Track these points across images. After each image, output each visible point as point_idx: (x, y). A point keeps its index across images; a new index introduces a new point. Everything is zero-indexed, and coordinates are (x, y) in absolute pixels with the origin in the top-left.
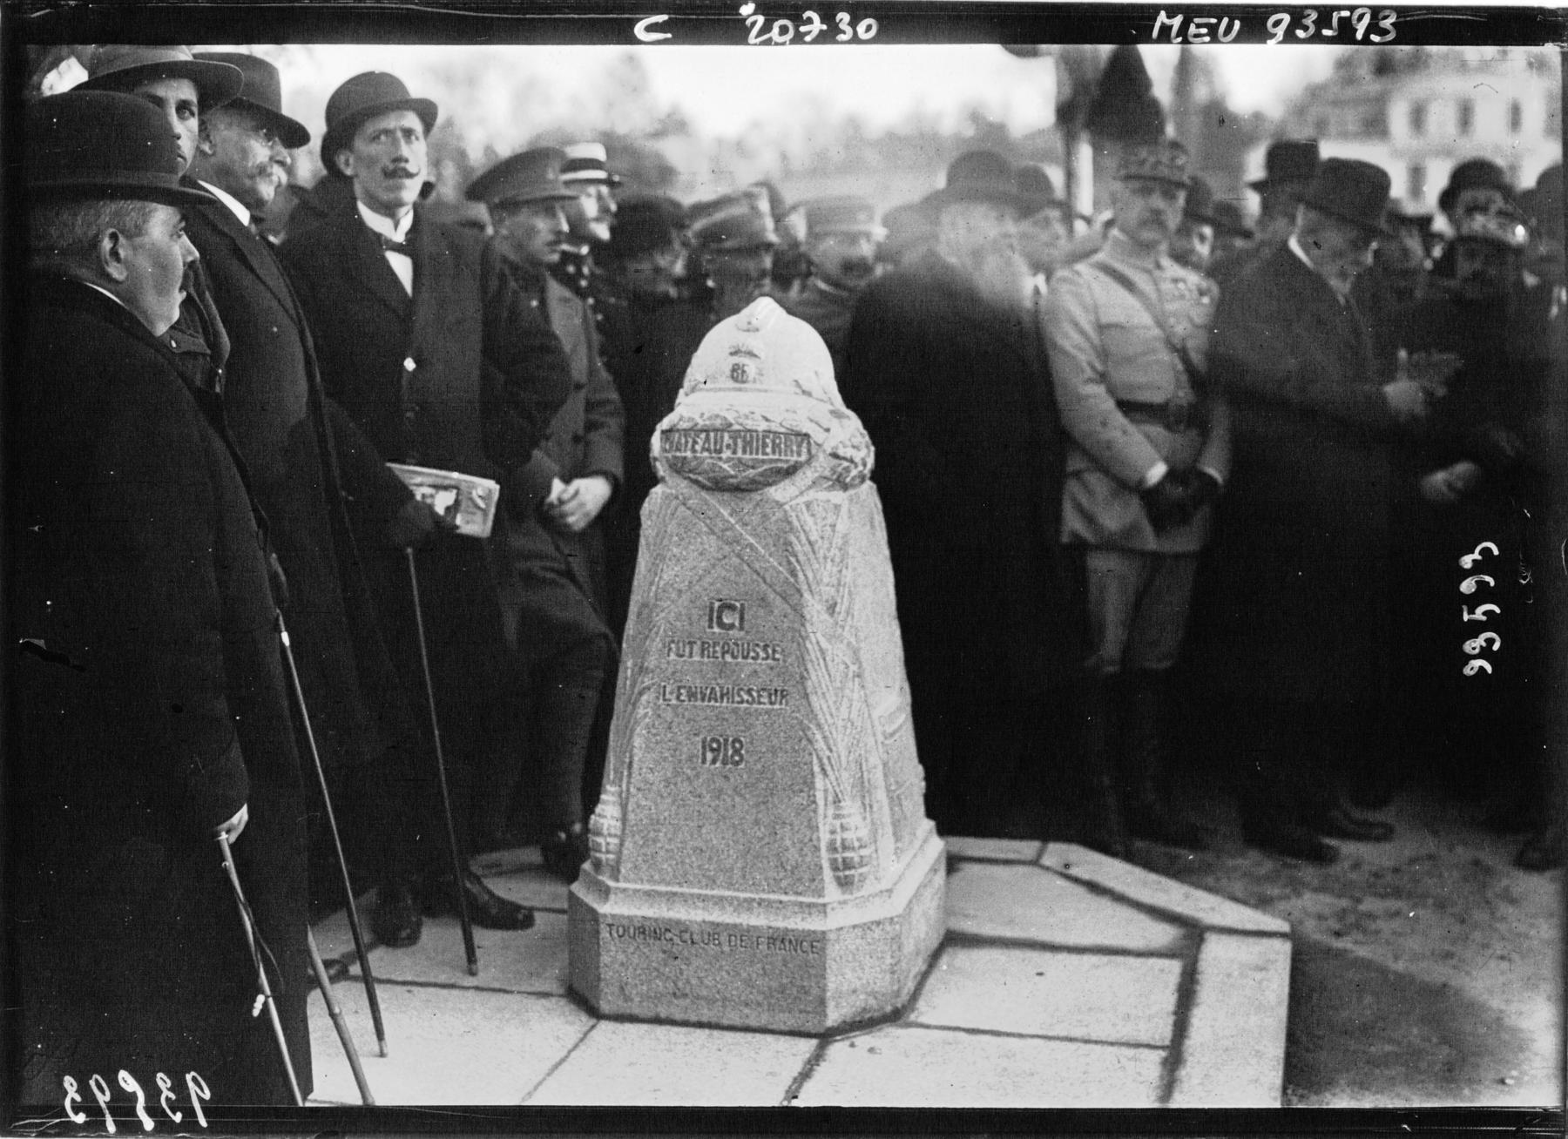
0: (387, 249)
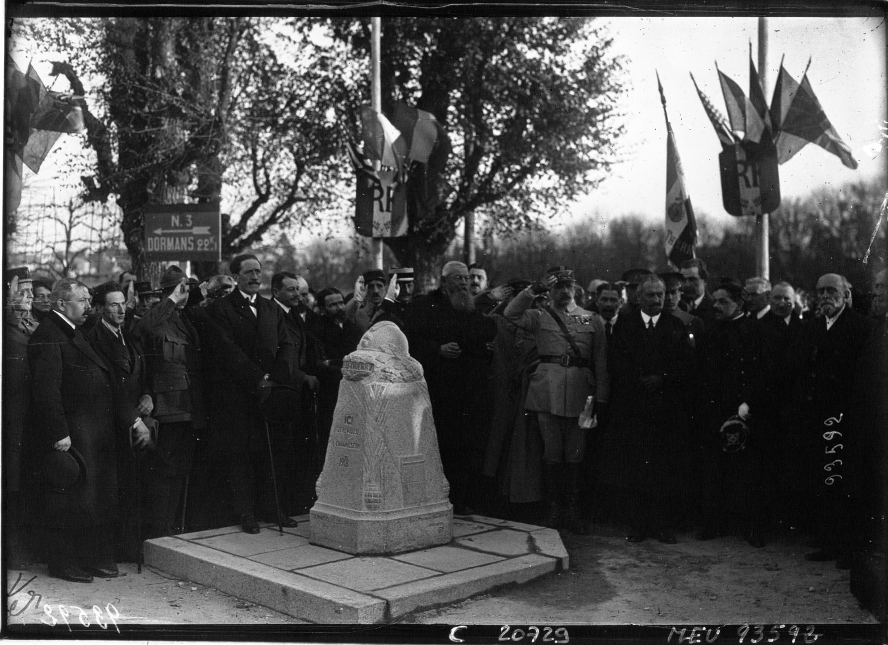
0: (116, 167)
